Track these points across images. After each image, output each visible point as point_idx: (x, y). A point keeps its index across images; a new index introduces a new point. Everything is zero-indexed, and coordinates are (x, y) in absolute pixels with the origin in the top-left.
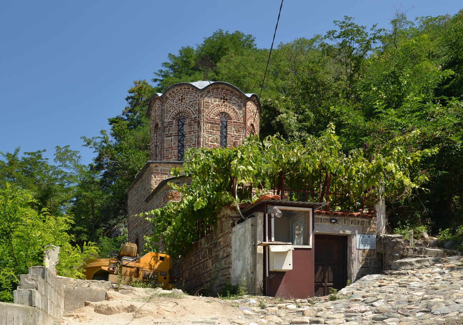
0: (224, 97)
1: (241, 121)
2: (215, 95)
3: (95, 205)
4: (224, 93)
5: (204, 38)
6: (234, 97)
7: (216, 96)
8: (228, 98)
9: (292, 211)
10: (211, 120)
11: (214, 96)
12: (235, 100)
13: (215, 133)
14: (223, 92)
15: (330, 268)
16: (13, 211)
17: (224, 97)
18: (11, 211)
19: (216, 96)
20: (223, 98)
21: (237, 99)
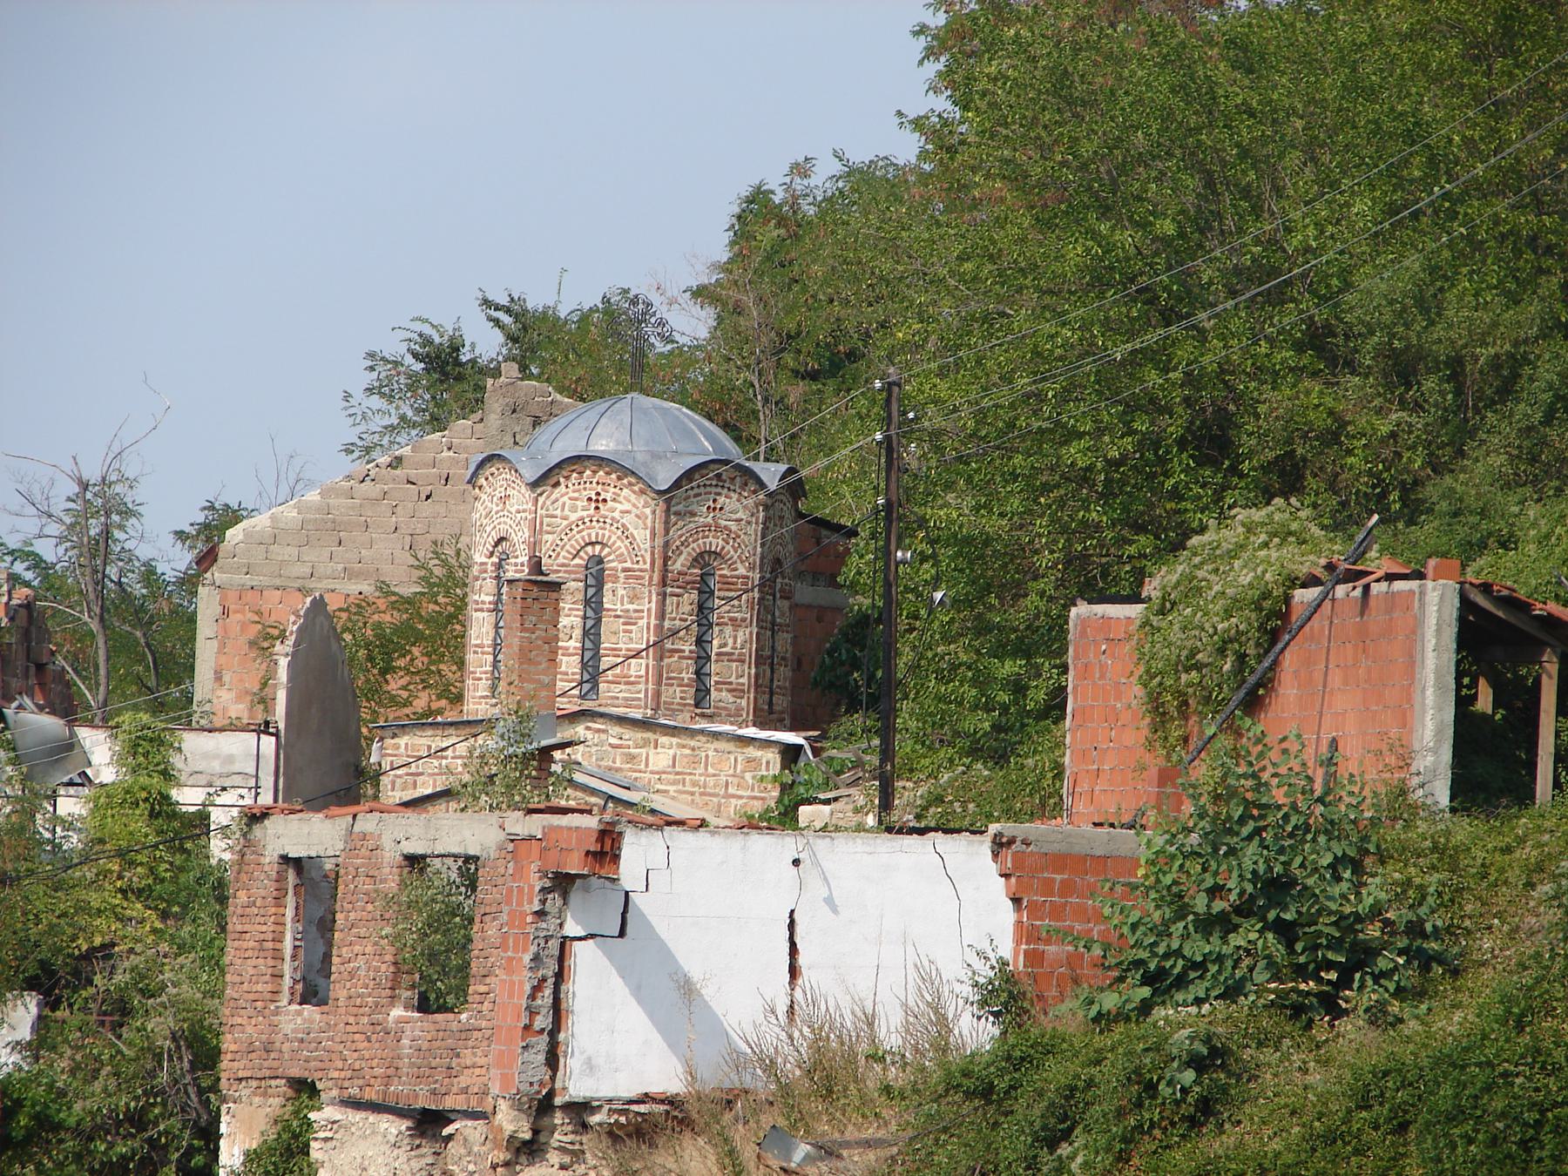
0: (598, 494)
1: (645, 563)
2: (574, 491)
3: (876, 742)
4: (598, 483)
5: (916, 34)
6: (625, 490)
7: (576, 495)
8: (608, 496)
9: (1411, 664)
10: (559, 571)
11: (571, 495)
12: (629, 501)
13: (570, 609)
14: (595, 480)
15: (1323, 974)
16: (1111, 263)
17: (598, 494)
18: (1302, 396)
19: (576, 495)
20: (594, 498)
21: (633, 497)
